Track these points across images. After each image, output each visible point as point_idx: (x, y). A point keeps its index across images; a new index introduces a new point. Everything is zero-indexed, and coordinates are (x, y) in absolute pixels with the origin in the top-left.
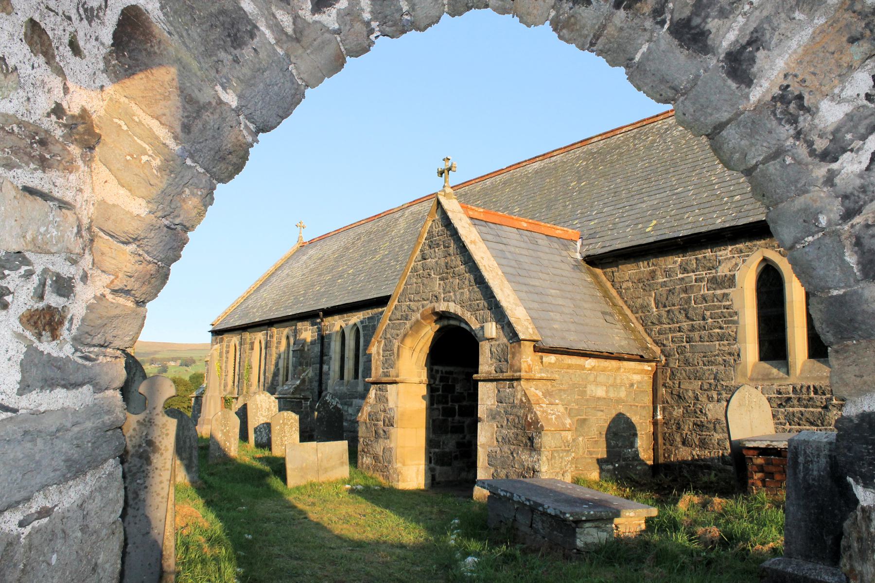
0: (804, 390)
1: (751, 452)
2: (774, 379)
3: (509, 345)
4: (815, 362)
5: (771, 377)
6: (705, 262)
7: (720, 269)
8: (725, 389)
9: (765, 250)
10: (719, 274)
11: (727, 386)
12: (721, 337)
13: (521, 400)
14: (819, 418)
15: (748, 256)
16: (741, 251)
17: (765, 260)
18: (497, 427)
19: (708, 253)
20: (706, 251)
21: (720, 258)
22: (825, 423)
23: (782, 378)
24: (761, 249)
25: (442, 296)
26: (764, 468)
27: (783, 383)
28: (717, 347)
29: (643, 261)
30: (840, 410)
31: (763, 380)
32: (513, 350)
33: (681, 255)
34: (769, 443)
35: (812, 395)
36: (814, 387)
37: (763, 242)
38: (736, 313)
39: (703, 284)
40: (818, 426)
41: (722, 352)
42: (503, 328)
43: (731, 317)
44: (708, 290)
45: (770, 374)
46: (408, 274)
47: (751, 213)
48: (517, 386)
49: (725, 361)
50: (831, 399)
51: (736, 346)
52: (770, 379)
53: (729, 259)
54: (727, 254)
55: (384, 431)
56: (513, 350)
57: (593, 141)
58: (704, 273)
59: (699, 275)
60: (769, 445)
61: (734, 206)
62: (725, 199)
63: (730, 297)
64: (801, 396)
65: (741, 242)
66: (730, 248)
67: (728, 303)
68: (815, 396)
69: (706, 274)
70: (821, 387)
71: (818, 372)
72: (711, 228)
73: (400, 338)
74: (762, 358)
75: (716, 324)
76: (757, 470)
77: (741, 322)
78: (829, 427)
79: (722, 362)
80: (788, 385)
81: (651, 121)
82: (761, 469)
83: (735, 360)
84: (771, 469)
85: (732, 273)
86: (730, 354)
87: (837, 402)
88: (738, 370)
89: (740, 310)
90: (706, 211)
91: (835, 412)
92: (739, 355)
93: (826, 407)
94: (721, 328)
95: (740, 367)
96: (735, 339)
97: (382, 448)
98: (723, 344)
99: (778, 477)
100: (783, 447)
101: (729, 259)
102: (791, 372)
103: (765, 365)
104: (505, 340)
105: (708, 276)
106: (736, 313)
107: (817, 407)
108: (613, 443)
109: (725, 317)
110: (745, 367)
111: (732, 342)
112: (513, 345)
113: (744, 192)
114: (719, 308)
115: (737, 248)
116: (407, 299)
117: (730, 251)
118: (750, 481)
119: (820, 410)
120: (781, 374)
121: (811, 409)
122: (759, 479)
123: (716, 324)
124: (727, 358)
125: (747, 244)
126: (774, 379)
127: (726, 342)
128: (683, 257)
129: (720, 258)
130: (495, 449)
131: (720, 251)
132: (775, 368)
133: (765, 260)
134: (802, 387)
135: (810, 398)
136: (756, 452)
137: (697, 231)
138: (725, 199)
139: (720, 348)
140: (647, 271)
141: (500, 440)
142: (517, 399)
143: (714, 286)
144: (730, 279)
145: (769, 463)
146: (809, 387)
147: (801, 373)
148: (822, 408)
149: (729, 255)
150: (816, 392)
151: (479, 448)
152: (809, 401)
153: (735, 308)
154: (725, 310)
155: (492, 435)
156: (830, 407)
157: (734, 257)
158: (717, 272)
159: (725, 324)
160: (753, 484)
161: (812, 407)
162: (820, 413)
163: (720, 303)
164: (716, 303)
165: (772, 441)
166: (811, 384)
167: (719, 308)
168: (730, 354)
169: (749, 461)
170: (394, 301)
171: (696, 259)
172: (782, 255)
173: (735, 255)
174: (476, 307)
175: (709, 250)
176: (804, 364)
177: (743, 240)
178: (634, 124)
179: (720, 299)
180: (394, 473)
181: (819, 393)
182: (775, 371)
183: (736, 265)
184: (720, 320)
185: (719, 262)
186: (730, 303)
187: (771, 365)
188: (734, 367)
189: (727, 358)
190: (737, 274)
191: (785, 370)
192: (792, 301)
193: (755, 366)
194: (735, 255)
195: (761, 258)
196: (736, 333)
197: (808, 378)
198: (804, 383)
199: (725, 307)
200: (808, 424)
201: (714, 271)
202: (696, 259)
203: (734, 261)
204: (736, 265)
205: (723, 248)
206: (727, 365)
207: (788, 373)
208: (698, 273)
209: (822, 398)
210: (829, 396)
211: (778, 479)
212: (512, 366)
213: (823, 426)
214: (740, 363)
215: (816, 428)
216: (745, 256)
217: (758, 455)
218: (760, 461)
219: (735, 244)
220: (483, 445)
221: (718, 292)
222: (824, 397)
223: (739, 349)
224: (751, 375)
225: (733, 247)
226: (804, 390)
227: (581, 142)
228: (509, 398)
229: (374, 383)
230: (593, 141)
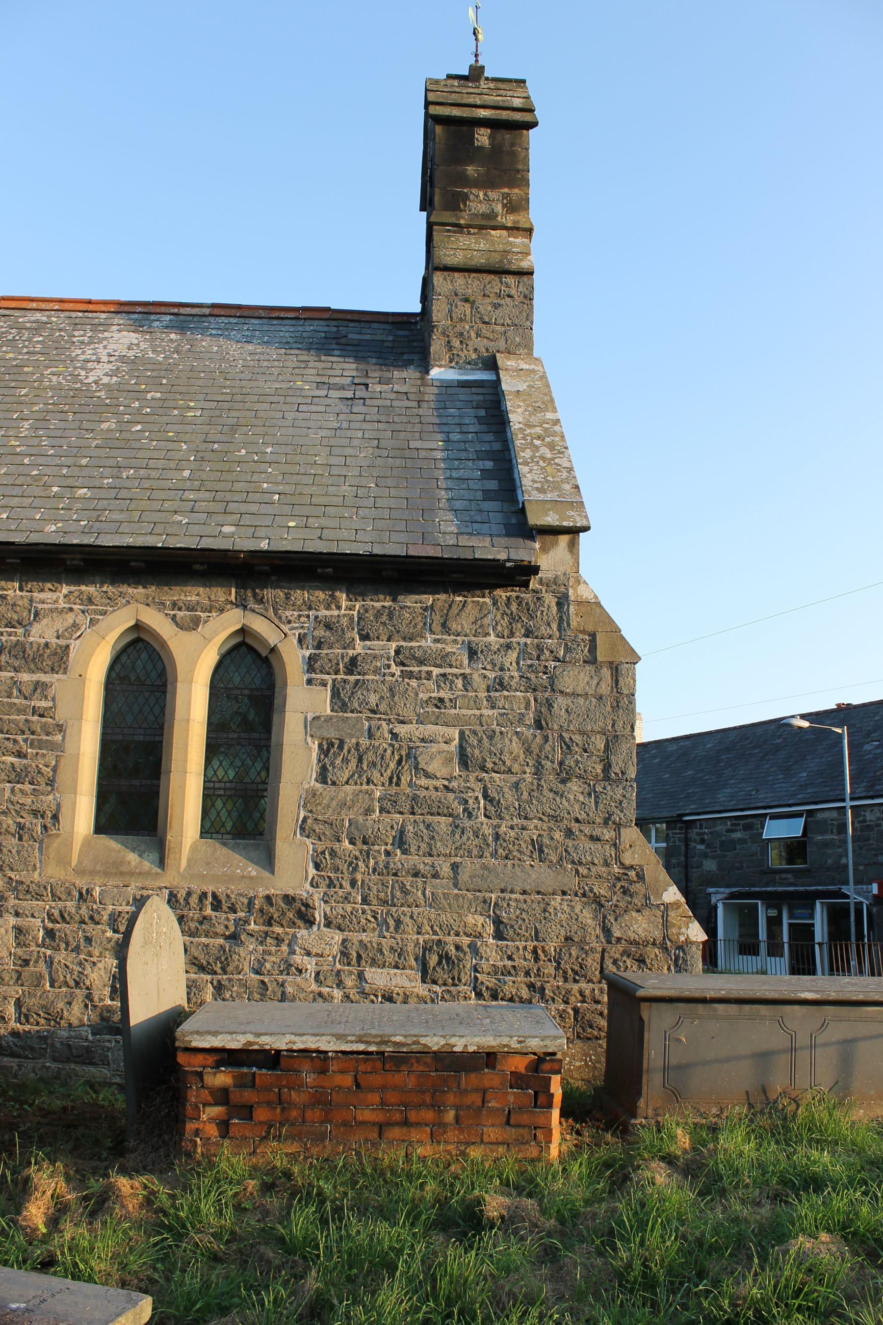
0: (194, 900)
1: (200, 1058)
2: (131, 874)
4: (218, 845)
5: (124, 869)
7: (36, 629)
8: (16, 889)
9: (142, 607)
10: (31, 639)
11: (22, 883)
12: (18, 775)
14: (218, 958)
15: (105, 613)
16: (90, 601)
17: (138, 627)
20: (10, 584)
21: (40, 606)
22: (230, 969)
23: (148, 873)
24: (134, 606)
26: (232, 1096)
27: (149, 883)
28: (7, 794)
29: (303, 589)
30: (261, 943)
31: (106, 874)
34: (250, 1038)
35: (208, 911)
36: (214, 896)
37: (141, 590)
38: (60, 728)
40: (215, 973)
41: (18, 807)
45: (122, 862)
47: (125, 528)
49: (21, 827)
50: (247, 922)
51: (51, 797)
52: (122, 874)
53: (61, 612)
54: (56, 601)
60: (250, 1043)
61: (79, 506)
62: (55, 489)
63: (51, 692)
64: (185, 912)
65: (93, 583)
66: (65, 589)
67: (44, 704)
68: (214, 914)
70: (228, 896)
71: (224, 866)
72: (34, 538)
74: (99, 829)
75: (10, 745)
76: (210, 1099)
77: (69, 747)
78: (236, 977)
79: (13, 828)
80: (160, 889)
82: (222, 1096)
83: (45, 827)
84: (248, 1096)
85: (62, 642)
86: (35, 813)
87: (257, 928)
89: (70, 723)
90: (14, 502)
91: (251, 947)
92: (55, 817)
93: (234, 937)
94: (20, 755)
95: (56, 843)
96: (51, 782)
98: (21, 791)
99: (261, 1114)
100: (284, 1047)
101: (61, 612)
102: (170, 861)
103: (110, 844)
106: (60, 728)
107: (216, 935)
109: (33, 733)
110: (69, 844)
111: (43, 787)
113: (97, 484)
114: (21, 711)
115: (82, 593)
117: (65, 596)
118: (190, 1126)
119: (221, 941)
120: (147, 865)
121: (204, 940)
122: (211, 1120)
123: (10, 745)
124: (27, 820)
125: (105, 589)
126: (131, 874)
127: (28, 787)
129: (40, 606)
131: (42, 590)
132: (133, 850)
133: (138, 627)
134: (189, 894)
135: (205, 918)
136: (211, 1059)
138: (55, 489)
139: (14, 799)
140: (278, 620)
143: (17, 664)
144: (55, 654)
145: (242, 1083)
146: (204, 895)
147: (189, 866)
148: (227, 938)
149: (62, 605)
150: (217, 905)
152: (201, 923)
153: (61, 715)
154: (36, 718)
156: (243, 937)
157: (71, 609)
158: (27, 634)
159: (32, 746)
160: (197, 1133)
161: (206, 936)
162: (222, 948)
163: (24, 702)
165: (259, 1035)
166: (210, 889)
167: (21, 711)
168: (35, 813)
169: (192, 1079)
172: (177, 624)
173: (76, 607)
175: (17, 585)
176: (194, 848)
177: (98, 579)
179: (27, 691)
181: (225, 908)
182: (132, 857)
183: (76, 626)
184: (20, 738)
185: (37, 614)
186: (50, 704)
187: (123, 844)
188: (41, 842)
189: (27, 820)
190: (74, 645)
191: (155, 856)
192: (188, 721)
193: (86, 843)
194: (76, 607)
195: (239, 627)
196: (55, 770)
197: (203, 877)
198: (194, 887)
199: (34, 711)
200: (195, 969)
201: (20, 631)
203: (70, 618)
204: (76, 626)
205: (49, 585)
206: (26, 837)
207: (162, 863)
209: (228, 919)
210: (243, 914)
211: (262, 1118)
213: (225, 973)
214: (58, 835)
215: (209, 977)
216: (96, 612)
217: (218, 1065)
218: (222, 1078)
222: (232, 916)
223: (59, 806)
224: (80, 862)
225: (73, 588)
226: (194, 900)
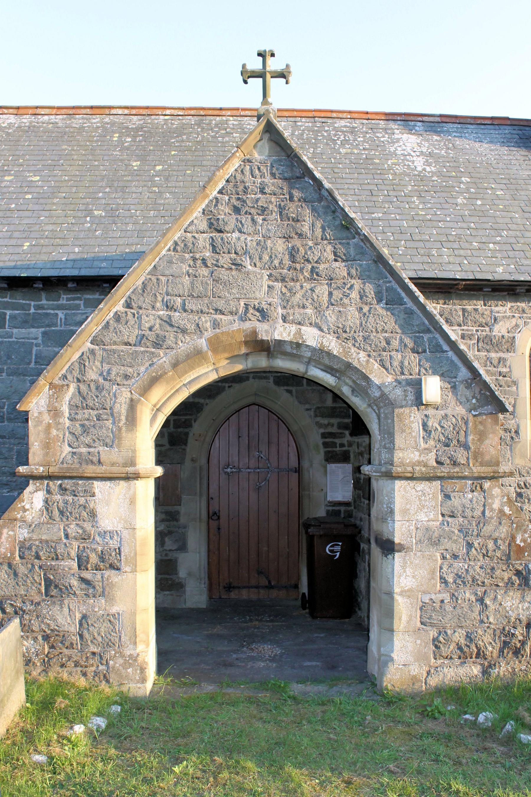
3: (471, 418)
6: (477, 317)
7: (496, 328)
10: (494, 334)
13: (501, 511)
18: (444, 558)
19: (479, 305)
21: (497, 315)
25: (280, 311)
32: (481, 427)
33: (441, 301)
38: (515, 383)
39: (473, 342)
42: (454, 388)
43: (509, 386)
44: (478, 351)
46: (164, 252)
48: (490, 488)
51: (513, 421)
54: (505, 312)
55: (83, 580)
56: (481, 427)
57: (113, 111)
58: (475, 329)
59: (467, 330)
63: (508, 363)
66: (509, 305)
67: (504, 370)
69: (477, 331)
73: (135, 383)
81: (210, 112)
83: (512, 438)
85: (511, 335)
88: (517, 450)
92: (517, 432)
95: (519, 446)
97: (78, 616)
104: (461, 411)
105: (479, 333)
108: (162, 528)
112: (479, 419)
116: (158, 305)
128: (445, 303)
130: (440, 596)
131: (497, 306)
137: (479, 276)
141: (450, 580)
142: (492, 510)
143: (488, 348)
149: (508, 314)
151: (397, 597)
154: (501, 378)
155: (433, 572)
157: (514, 316)
164: (489, 368)
170: (114, 305)
171: (464, 310)
174: (384, 344)
177: (526, 299)
178: (183, 109)
180: (127, 664)
183: (517, 326)
186: (508, 370)
190: (518, 336)
196: (514, 406)
202: (464, 310)
203: (514, 321)
205: (500, 303)
208: (465, 328)
212: (477, 455)
214: (519, 442)
219: (516, 302)
220: (407, 593)
221: (493, 355)
223: (518, 426)
225: (513, 304)
227: (92, 108)
228: (472, 510)
229: (36, 478)
230: (113, 111)
